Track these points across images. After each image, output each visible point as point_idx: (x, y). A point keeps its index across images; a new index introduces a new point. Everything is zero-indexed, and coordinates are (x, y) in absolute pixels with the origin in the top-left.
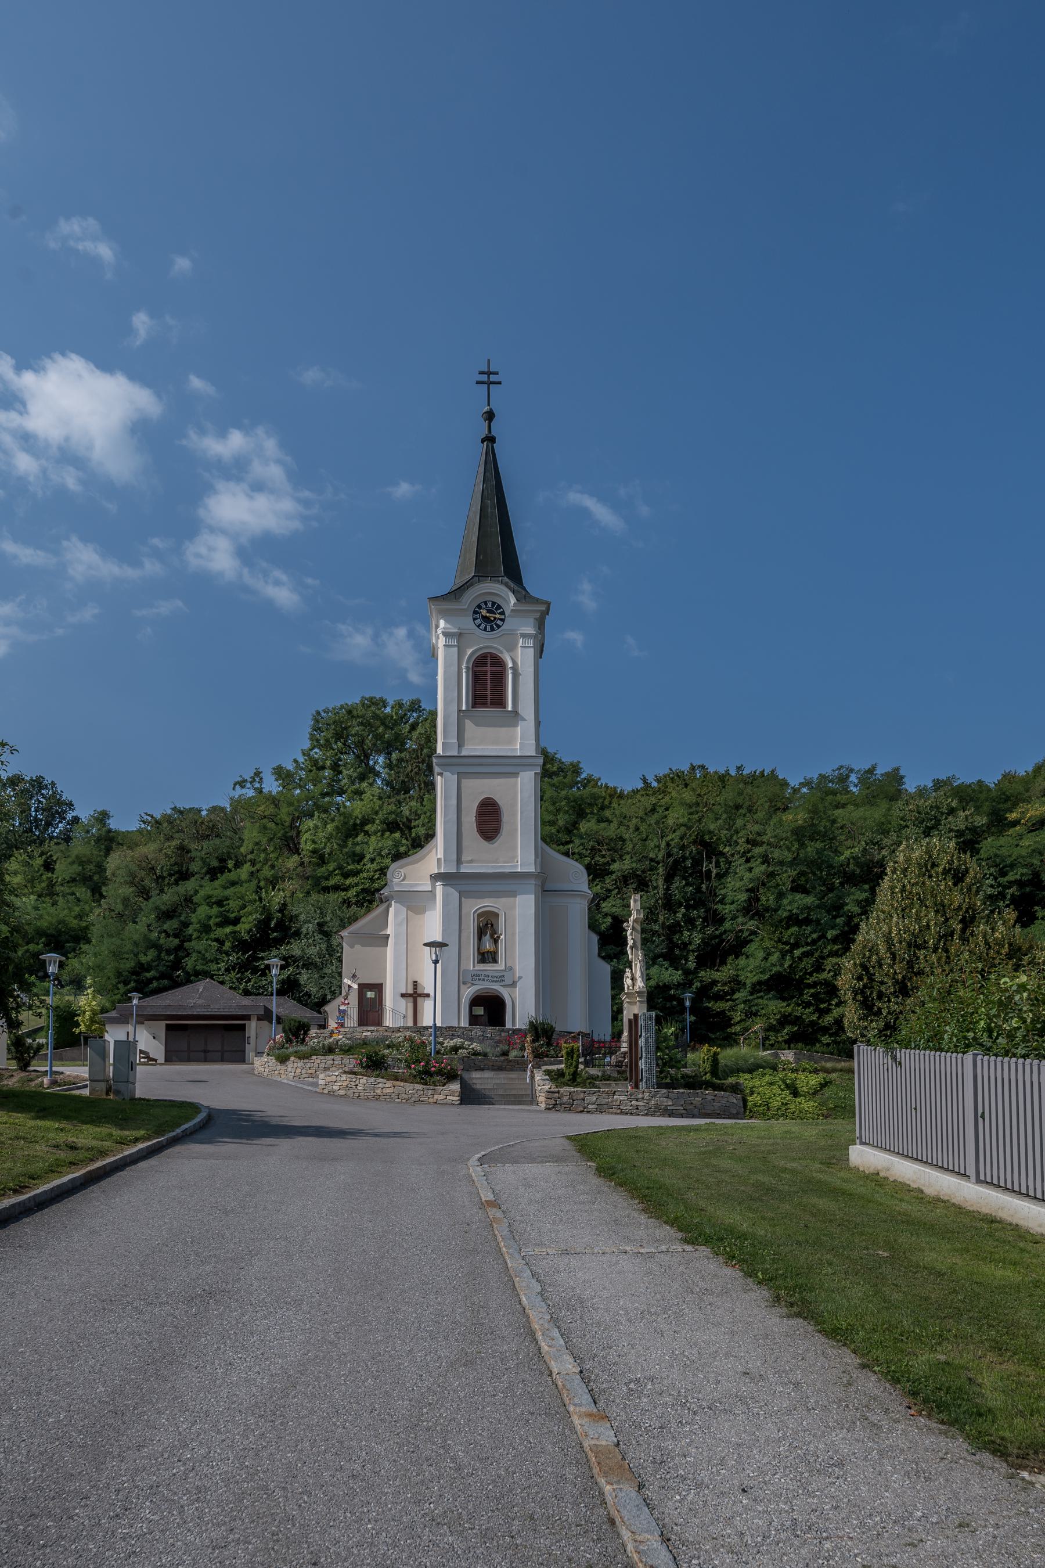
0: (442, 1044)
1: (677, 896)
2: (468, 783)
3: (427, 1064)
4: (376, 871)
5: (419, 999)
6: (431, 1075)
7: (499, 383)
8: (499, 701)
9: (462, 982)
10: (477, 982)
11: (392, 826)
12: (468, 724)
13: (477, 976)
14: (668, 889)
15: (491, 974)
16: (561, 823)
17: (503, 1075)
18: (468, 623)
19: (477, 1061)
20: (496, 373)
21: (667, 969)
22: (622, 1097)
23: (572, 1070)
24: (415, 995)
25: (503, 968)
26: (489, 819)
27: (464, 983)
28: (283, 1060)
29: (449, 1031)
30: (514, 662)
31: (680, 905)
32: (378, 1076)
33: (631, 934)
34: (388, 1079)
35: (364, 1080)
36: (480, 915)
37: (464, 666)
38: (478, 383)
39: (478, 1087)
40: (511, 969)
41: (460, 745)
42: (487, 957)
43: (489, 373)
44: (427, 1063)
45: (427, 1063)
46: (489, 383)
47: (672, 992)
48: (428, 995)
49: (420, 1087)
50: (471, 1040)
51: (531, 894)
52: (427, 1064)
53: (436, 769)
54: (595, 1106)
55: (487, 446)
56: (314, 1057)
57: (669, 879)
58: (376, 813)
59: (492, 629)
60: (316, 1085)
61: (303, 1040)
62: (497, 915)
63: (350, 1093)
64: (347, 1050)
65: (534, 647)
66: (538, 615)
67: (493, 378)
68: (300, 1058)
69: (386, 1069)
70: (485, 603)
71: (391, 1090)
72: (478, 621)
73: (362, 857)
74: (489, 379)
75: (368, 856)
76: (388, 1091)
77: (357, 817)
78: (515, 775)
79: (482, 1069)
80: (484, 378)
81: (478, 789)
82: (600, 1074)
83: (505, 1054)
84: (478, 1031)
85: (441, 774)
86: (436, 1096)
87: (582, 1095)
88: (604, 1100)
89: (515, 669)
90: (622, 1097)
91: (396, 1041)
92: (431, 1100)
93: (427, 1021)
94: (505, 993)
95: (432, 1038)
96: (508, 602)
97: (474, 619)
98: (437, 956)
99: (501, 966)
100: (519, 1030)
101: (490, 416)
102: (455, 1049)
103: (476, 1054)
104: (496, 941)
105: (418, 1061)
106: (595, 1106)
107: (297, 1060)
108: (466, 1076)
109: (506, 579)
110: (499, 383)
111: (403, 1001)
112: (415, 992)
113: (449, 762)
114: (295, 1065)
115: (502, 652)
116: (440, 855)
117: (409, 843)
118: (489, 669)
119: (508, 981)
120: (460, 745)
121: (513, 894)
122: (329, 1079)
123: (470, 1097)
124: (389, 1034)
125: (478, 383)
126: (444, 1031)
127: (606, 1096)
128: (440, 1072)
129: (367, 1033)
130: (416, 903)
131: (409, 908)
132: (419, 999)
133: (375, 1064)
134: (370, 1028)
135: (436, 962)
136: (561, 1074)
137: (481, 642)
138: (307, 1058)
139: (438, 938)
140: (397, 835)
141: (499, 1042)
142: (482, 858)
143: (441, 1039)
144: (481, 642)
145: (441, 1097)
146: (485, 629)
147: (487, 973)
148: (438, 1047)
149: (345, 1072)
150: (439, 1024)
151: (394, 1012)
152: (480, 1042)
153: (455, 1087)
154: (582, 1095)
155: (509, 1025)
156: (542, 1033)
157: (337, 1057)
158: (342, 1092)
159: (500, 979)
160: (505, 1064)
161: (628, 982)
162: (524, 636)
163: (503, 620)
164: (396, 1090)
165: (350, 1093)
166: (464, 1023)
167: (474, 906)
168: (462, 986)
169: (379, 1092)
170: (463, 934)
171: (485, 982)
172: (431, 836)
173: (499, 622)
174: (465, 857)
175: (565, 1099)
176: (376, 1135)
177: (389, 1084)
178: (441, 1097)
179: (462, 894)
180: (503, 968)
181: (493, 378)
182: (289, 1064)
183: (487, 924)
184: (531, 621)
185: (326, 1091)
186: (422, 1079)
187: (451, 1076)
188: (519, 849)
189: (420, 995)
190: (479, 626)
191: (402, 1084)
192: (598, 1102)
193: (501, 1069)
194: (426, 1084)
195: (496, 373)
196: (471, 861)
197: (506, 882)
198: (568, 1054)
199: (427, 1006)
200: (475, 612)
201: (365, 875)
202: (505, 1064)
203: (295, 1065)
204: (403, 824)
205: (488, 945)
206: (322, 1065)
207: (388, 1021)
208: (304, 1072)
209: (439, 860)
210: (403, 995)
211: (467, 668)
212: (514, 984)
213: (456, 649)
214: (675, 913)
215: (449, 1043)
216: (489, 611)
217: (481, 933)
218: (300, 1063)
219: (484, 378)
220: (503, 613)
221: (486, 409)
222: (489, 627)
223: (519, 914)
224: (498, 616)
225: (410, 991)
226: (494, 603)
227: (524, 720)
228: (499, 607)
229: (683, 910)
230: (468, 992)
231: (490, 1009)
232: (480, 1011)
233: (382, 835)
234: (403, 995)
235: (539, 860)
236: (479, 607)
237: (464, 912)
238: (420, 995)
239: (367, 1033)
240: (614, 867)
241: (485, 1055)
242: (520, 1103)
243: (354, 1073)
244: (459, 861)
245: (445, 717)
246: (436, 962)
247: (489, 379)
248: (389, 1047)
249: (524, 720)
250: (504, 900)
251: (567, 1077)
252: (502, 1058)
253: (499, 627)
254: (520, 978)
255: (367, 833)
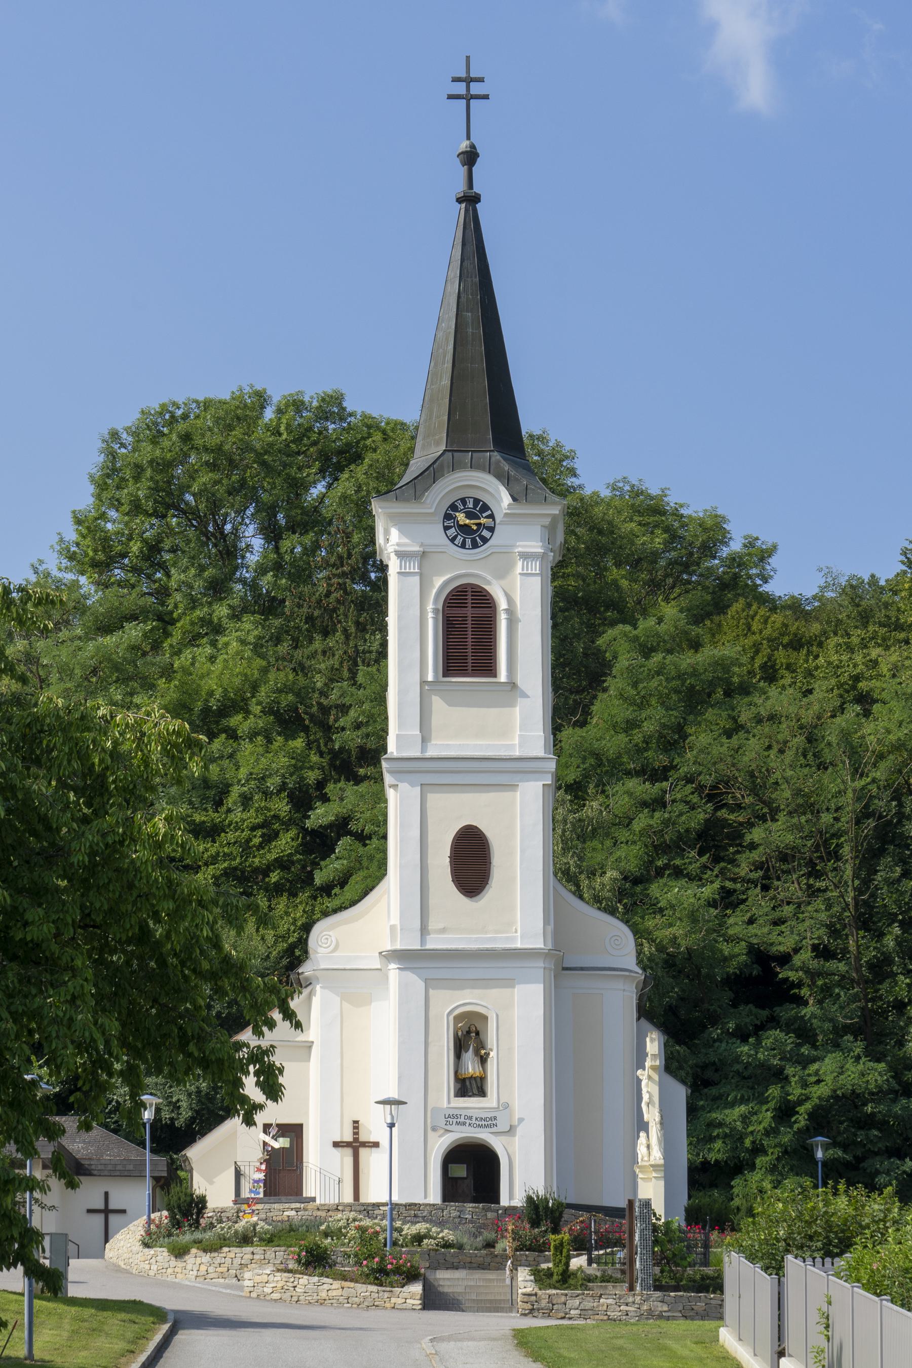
0: (399, 1230)
1: (886, 899)
2: (435, 799)
3: (383, 1256)
4: (253, 828)
5: (363, 1152)
6: (387, 1274)
7: (486, 97)
8: (487, 667)
9: (431, 1128)
10: (454, 1127)
11: (288, 722)
12: (437, 703)
13: (453, 1119)
14: (867, 882)
15: (475, 1114)
16: (649, 727)
17: (478, 1275)
18: (436, 535)
19: (448, 1255)
20: (481, 80)
21: (858, 1058)
22: (610, 1301)
23: (561, 1268)
24: (355, 1145)
25: (495, 1105)
26: (471, 862)
27: (434, 1129)
28: (179, 1252)
29: (412, 1211)
30: (510, 600)
31: (892, 918)
32: (321, 1275)
33: (647, 1085)
34: (334, 1279)
35: (304, 1280)
36: (458, 1019)
37: (430, 607)
38: (450, 97)
39: (446, 1290)
40: (507, 1106)
41: (425, 740)
42: (469, 1086)
43: (469, 80)
44: (383, 1259)
45: (383, 1259)
46: (469, 98)
47: (869, 1109)
48: (376, 1145)
49: (374, 1288)
50: (441, 1224)
51: (539, 983)
52: (383, 1256)
53: (388, 779)
54: (578, 1312)
55: (467, 210)
56: (225, 1249)
57: (869, 860)
58: (255, 688)
59: (475, 545)
60: (241, 1288)
61: (197, 1221)
62: (485, 1018)
63: (287, 1296)
64: (270, 1240)
65: (541, 574)
66: (547, 521)
67: (475, 89)
68: (205, 1251)
69: (330, 1266)
70: (463, 501)
71: (339, 1292)
72: (452, 532)
73: (224, 790)
74: (468, 90)
75: (236, 791)
76: (334, 1293)
77: (211, 694)
78: (513, 787)
79: (455, 1267)
80: (461, 88)
81: (455, 812)
82: (599, 1274)
83: (490, 1245)
84: (452, 1210)
85: (395, 787)
86: (393, 1300)
87: (563, 1299)
88: (588, 1304)
89: (510, 612)
90: (610, 1301)
91: (335, 1226)
92: (387, 1305)
93: (376, 1191)
94: (497, 1144)
95: (386, 1223)
96: (499, 501)
97: (446, 528)
98: (392, 1117)
99: (490, 1101)
100: (514, 1208)
101: (470, 158)
102: (418, 1239)
103: (447, 1245)
104: (483, 1060)
105: (371, 1257)
106: (578, 1312)
107: (200, 1253)
108: (430, 1276)
109: (496, 456)
110: (486, 97)
111: (337, 1152)
112: (356, 1140)
113: (411, 767)
114: (197, 1260)
115: (489, 583)
116: (395, 920)
117: (325, 761)
118: (469, 612)
119: (503, 1126)
120: (425, 740)
121: (509, 983)
122: (258, 1279)
123: (433, 1300)
124: (323, 1214)
125: (450, 97)
126: (402, 1210)
127: (591, 1299)
128: (397, 1271)
129: (287, 1211)
130: (355, 986)
131: (344, 997)
132: (363, 1152)
133: (316, 1260)
134: (294, 1205)
135: (391, 1126)
136: (549, 1274)
137: (457, 566)
138: (216, 1250)
139: (394, 1094)
140: (298, 743)
141: (484, 1226)
142: (463, 923)
143: (398, 1224)
144: (457, 566)
145: (400, 1301)
146: (463, 546)
147: (469, 1113)
148: (395, 1235)
149: (278, 1270)
150: (395, 1199)
151: (323, 1177)
152: (455, 1228)
153: (416, 1288)
154: (563, 1299)
155: (504, 1201)
156: (541, 1213)
157: (258, 1250)
158: (276, 1296)
159: (489, 1122)
160: (488, 1260)
161: (642, 1150)
162: (525, 556)
163: (492, 530)
164: (346, 1293)
165: (287, 1296)
166: (434, 1196)
167: (451, 1002)
168: (431, 1134)
169: (323, 1295)
170: (431, 1049)
171: (466, 1128)
172: (377, 870)
173: (486, 533)
174: (432, 925)
175: (544, 1303)
176: (340, 1329)
177: (337, 1284)
178: (400, 1301)
179: (429, 984)
180: (495, 1105)
181: (475, 89)
182: (190, 1259)
183: (469, 1032)
184: (537, 530)
185: (254, 1295)
186: (377, 1278)
187: (411, 1276)
188: (520, 903)
189: (364, 1144)
190: (453, 540)
191: (352, 1284)
192: (582, 1307)
193: (482, 1267)
194: (381, 1285)
195: (481, 80)
196: (443, 930)
197: (496, 962)
198: (556, 1248)
199: (375, 1164)
200: (447, 517)
201: (231, 836)
202: (488, 1260)
203: (198, 1260)
204: (312, 716)
205: (471, 1067)
206: (237, 1261)
207: (311, 1187)
208: (211, 1270)
209: (393, 928)
210: (336, 1145)
211: (436, 611)
212: (511, 1131)
213: (417, 579)
214: (881, 935)
215: (410, 1230)
216: (469, 515)
217: (460, 1047)
218: (206, 1258)
219: (461, 88)
220: (492, 516)
221: (464, 145)
222: (469, 542)
223: (520, 1019)
224: (483, 521)
225: (349, 1138)
226: (477, 501)
227: (525, 696)
228: (485, 508)
229: (897, 930)
230: (441, 1144)
231: (472, 1170)
232: (460, 1171)
233: (269, 741)
234: (336, 1145)
235: (550, 928)
236: (453, 507)
237: (432, 1013)
238: (364, 1144)
239: (287, 1211)
240: (756, 834)
241: (460, 1247)
242: (497, 1310)
243: (290, 1271)
244: (424, 930)
245: (401, 693)
246: (391, 1126)
247: (468, 90)
248: (326, 1235)
249: (525, 696)
250: (495, 993)
251: (555, 1277)
252: (484, 1252)
253: (485, 540)
254: (521, 1120)
255: (233, 735)
